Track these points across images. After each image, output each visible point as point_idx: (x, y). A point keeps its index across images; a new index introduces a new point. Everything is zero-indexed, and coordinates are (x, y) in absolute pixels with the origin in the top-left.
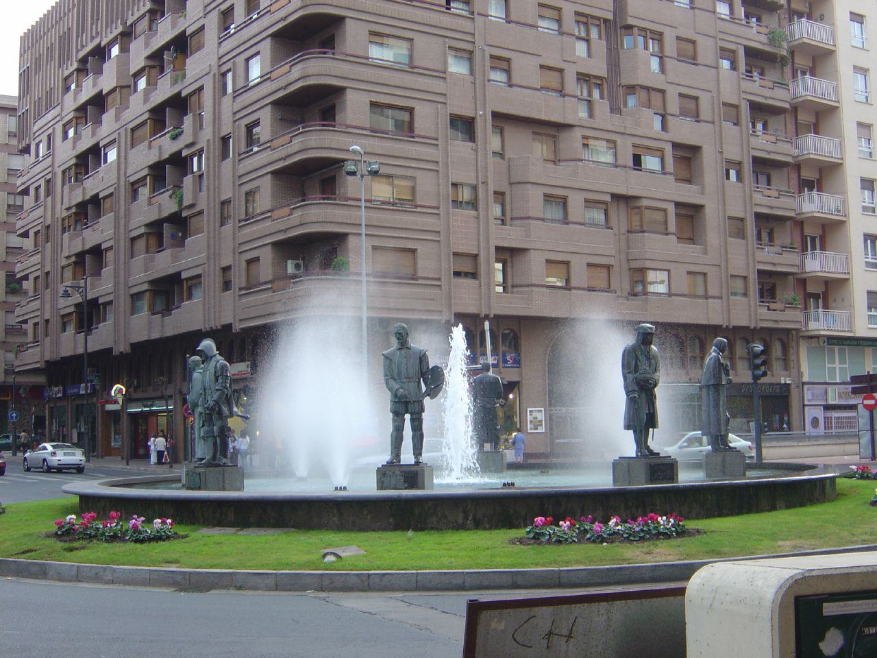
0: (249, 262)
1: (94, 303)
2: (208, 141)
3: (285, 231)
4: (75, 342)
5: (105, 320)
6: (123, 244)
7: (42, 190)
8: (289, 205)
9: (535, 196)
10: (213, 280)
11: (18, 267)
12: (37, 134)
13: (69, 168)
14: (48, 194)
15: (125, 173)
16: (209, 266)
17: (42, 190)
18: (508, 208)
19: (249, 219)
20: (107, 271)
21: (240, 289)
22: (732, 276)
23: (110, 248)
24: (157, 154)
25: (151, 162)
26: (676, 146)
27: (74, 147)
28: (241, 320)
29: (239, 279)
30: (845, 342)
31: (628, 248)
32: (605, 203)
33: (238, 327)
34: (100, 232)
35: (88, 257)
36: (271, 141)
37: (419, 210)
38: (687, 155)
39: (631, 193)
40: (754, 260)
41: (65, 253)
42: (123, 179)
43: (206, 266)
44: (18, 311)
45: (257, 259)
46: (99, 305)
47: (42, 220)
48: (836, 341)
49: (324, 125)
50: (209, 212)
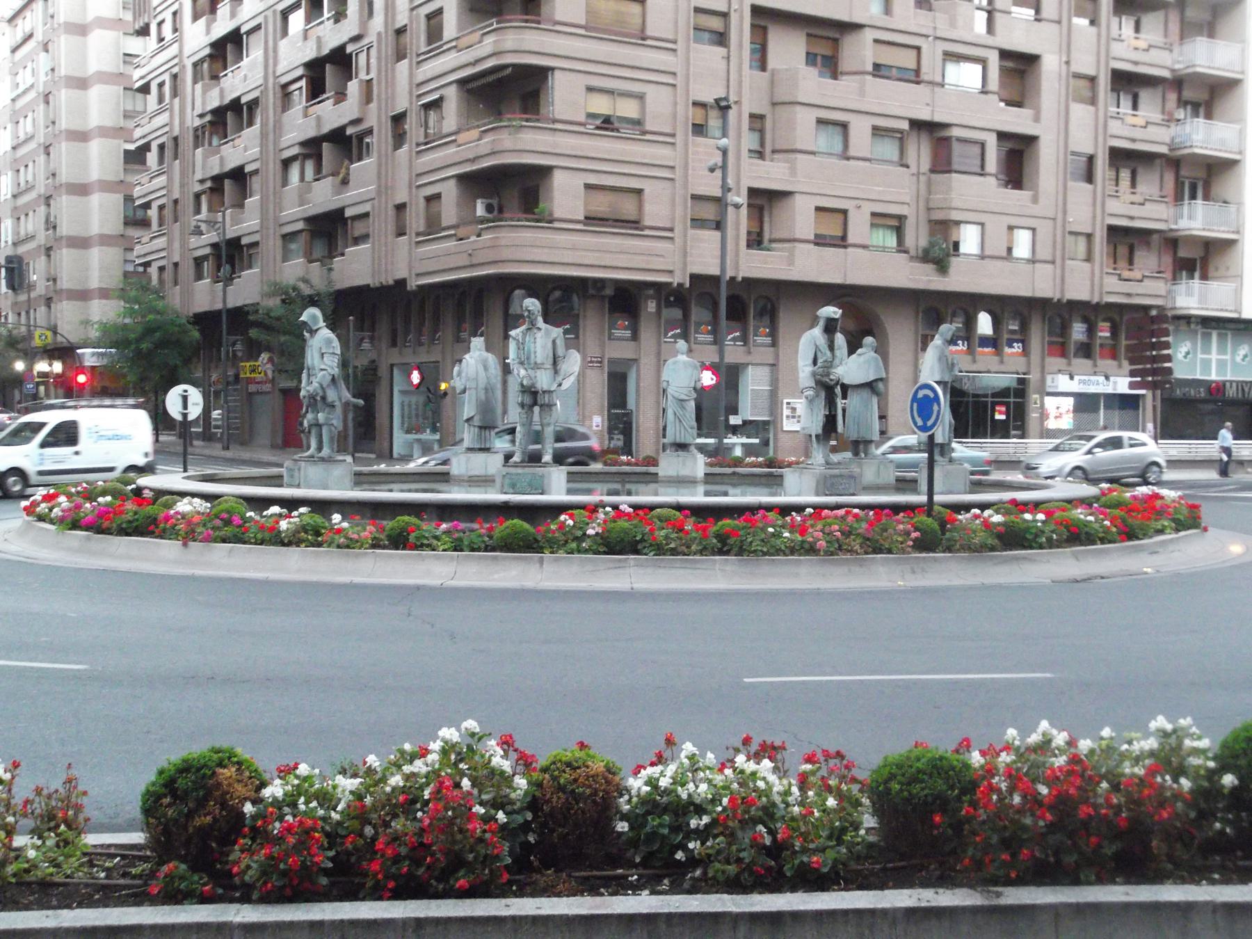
0: (429, 199)
1: (234, 244)
2: (379, 34)
3: (473, 160)
4: (213, 292)
5: (250, 267)
6: (274, 168)
7: (167, 89)
8: (478, 127)
9: (805, 118)
10: (382, 224)
11: (137, 192)
12: (159, 9)
13: (202, 61)
14: (175, 93)
15: (274, 72)
16: (380, 202)
17: (167, 89)
18: (768, 136)
19: (429, 143)
20: (252, 201)
21: (418, 234)
22: (1071, 233)
23: (256, 172)
24: (315, 47)
25: (307, 59)
26: (1005, 54)
27: (208, 32)
28: (418, 275)
29: (416, 220)
30: (1227, 325)
31: (930, 193)
32: (901, 131)
33: (413, 284)
34: (242, 149)
35: (227, 182)
36: (457, 39)
37: (648, 137)
38: (1019, 68)
39: (938, 118)
40: (1103, 211)
41: (199, 176)
42: (271, 80)
43: (376, 202)
44: (138, 250)
45: (437, 197)
46: (242, 247)
47: (166, 129)
48: (1214, 324)
49: (527, 21)
50: (380, 131)
